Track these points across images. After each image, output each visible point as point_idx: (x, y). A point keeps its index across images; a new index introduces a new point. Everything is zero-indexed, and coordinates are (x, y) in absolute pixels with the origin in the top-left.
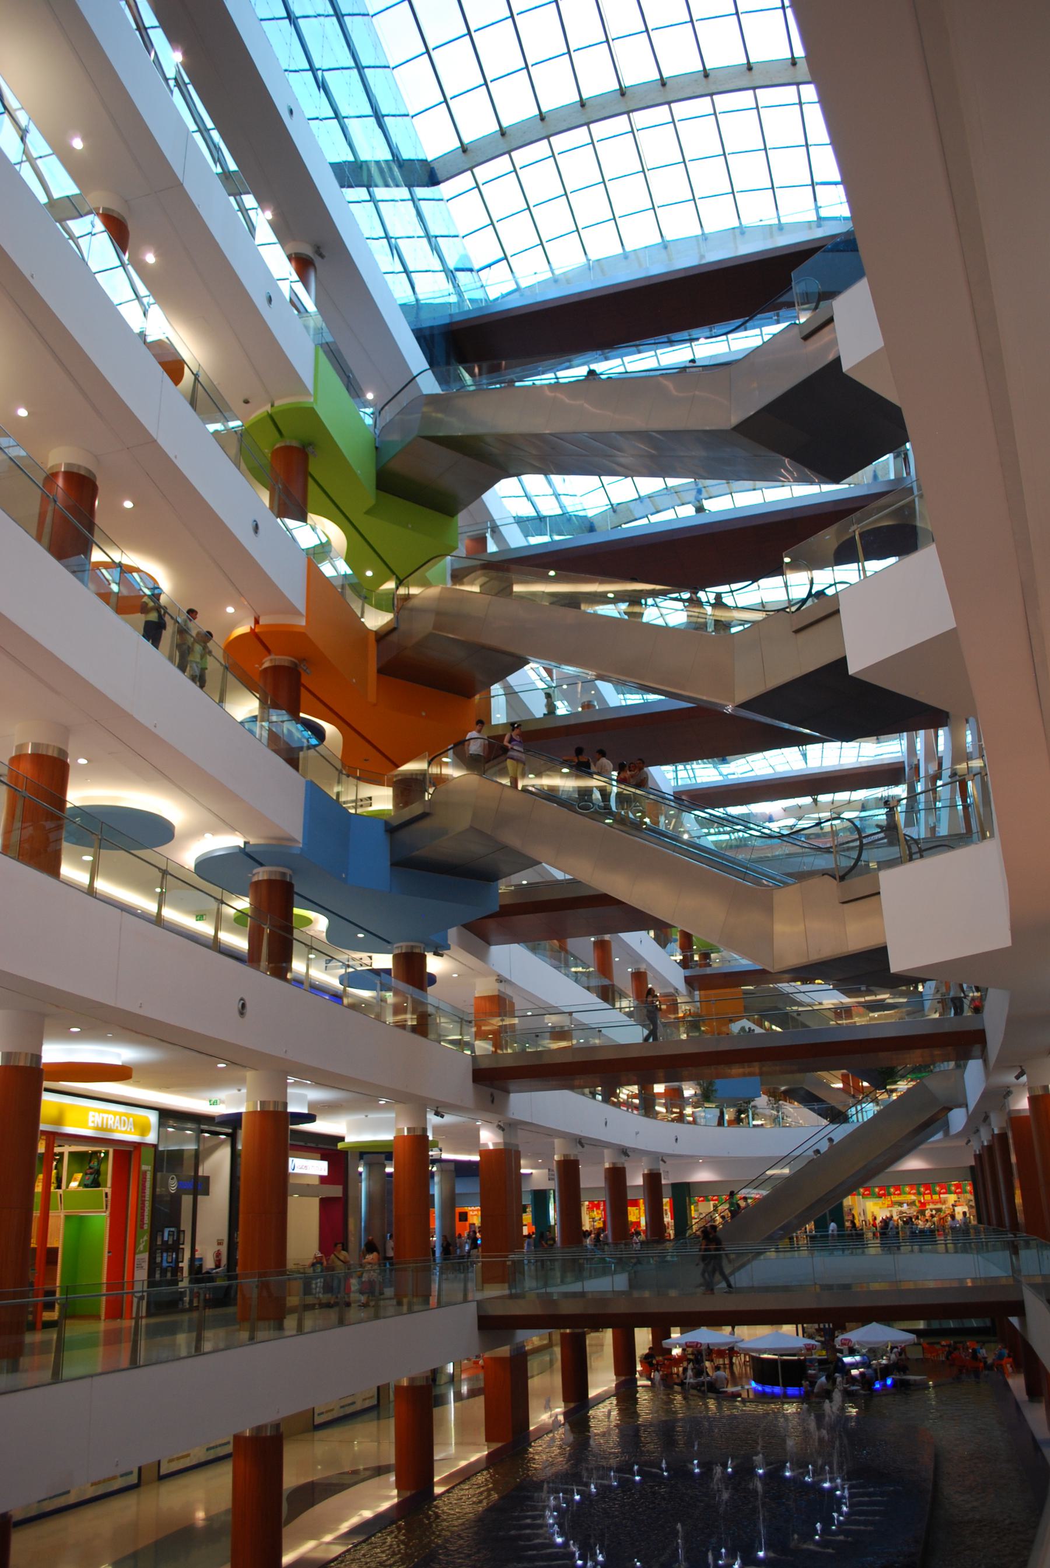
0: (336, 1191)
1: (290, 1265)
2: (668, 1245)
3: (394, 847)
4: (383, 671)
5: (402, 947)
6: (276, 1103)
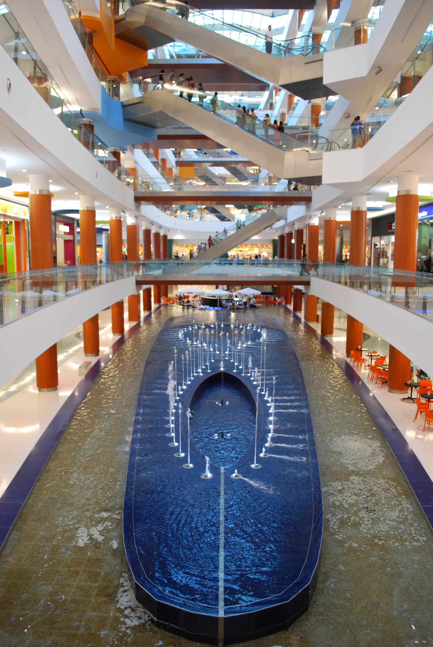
0: (70, 237)
1: (58, 265)
2: (59, 270)
3: (124, 112)
4: (117, 36)
5: (112, 149)
6: (91, 207)
